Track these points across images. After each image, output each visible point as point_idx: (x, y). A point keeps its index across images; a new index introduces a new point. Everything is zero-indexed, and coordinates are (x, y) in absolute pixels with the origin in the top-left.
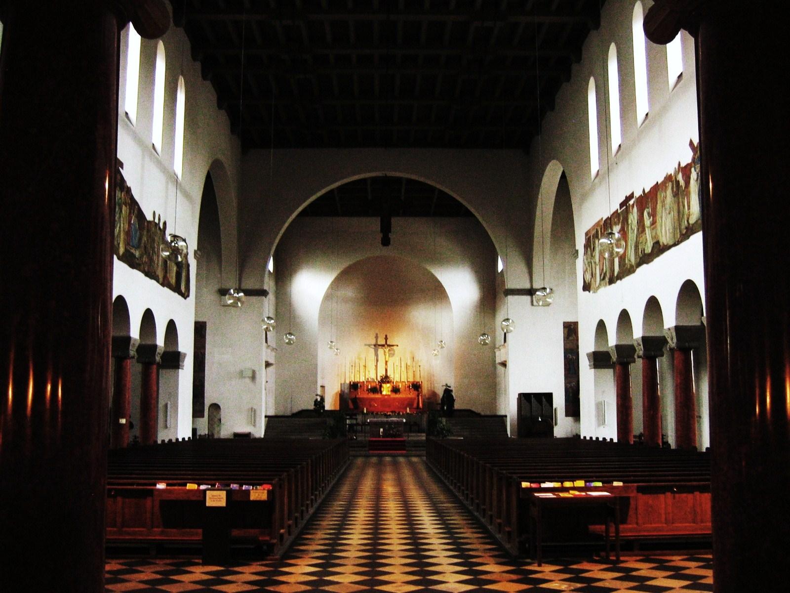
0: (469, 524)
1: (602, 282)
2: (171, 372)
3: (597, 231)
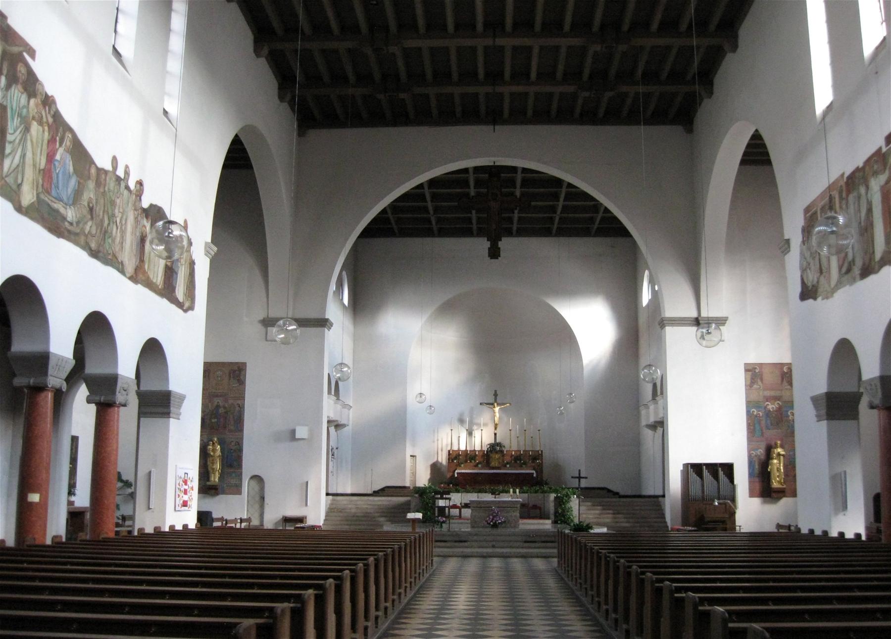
0: (570, 602)
1: (846, 277)
2: (159, 422)
3: (831, 199)
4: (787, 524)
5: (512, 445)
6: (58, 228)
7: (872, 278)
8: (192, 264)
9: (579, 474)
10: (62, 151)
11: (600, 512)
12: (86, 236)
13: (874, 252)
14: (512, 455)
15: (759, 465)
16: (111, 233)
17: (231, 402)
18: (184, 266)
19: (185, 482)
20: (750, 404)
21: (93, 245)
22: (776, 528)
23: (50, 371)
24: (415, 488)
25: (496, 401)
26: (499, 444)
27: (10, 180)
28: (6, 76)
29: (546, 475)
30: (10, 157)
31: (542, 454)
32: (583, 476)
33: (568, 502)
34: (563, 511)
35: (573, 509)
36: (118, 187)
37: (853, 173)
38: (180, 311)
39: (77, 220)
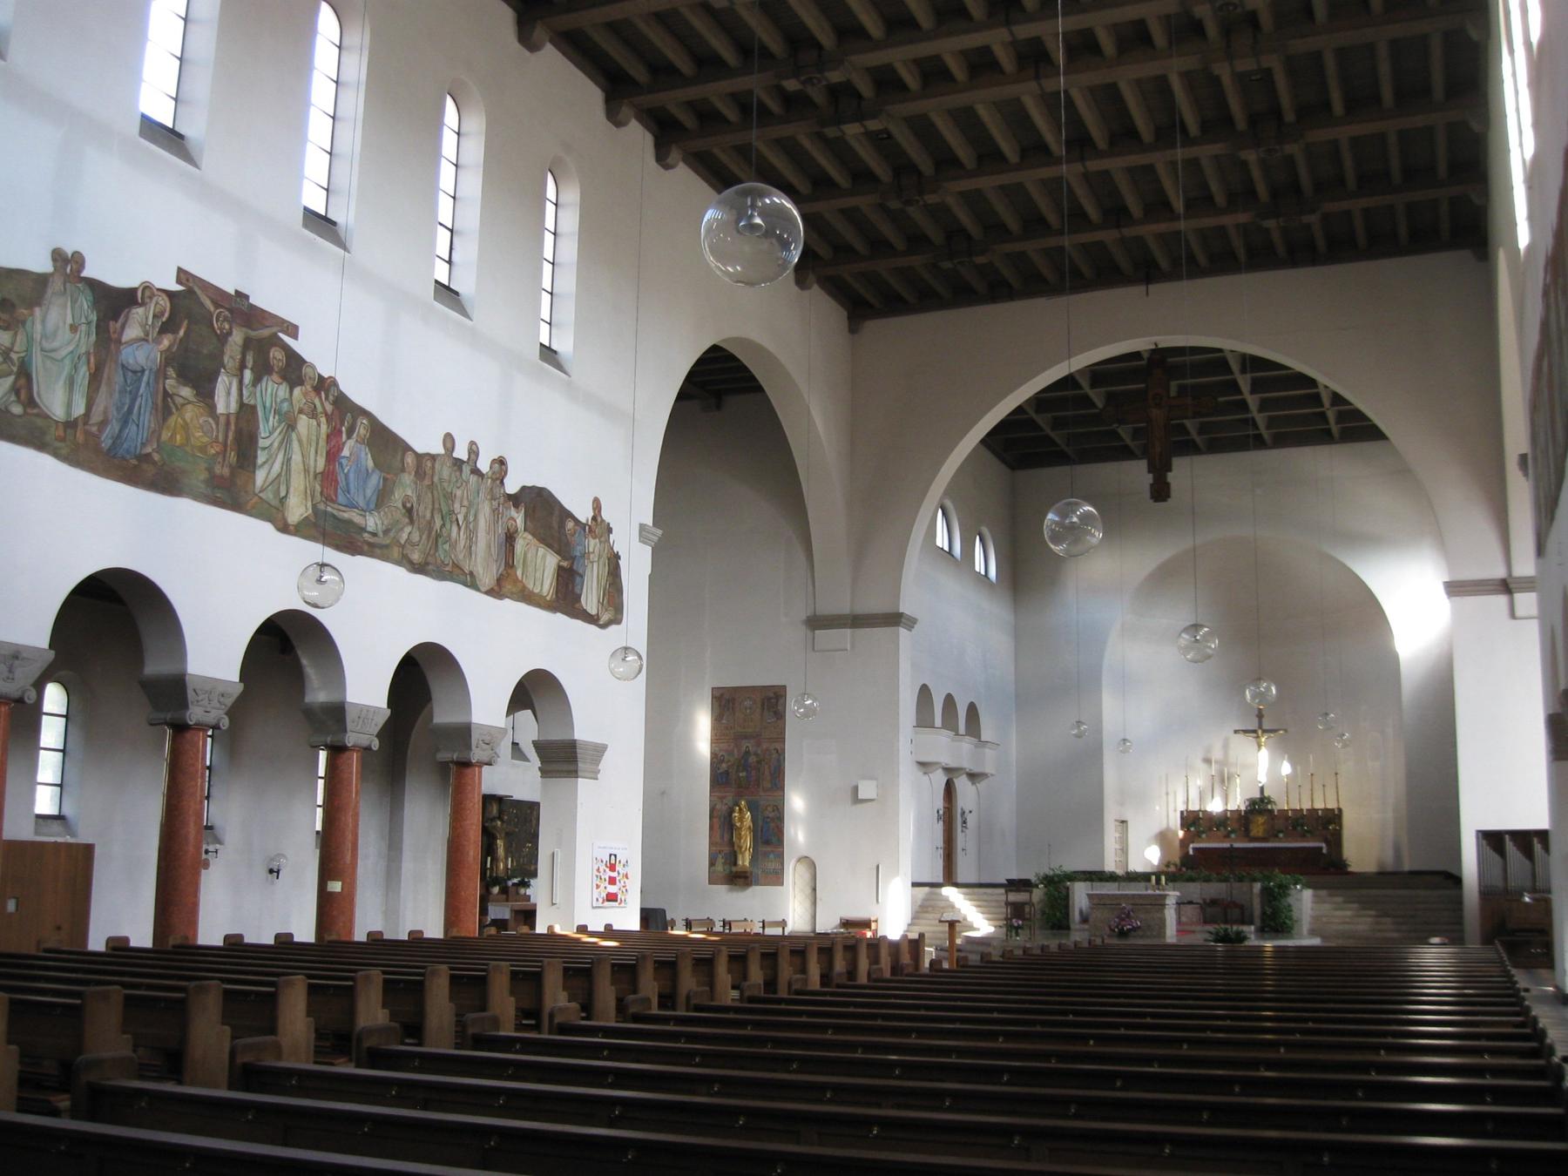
6: (351, 543)
8: (614, 561)
10: (353, 444)
12: (403, 547)
16: (449, 536)
17: (765, 746)
18: (595, 565)
19: (612, 868)
21: (416, 557)
23: (350, 726)
25: (1260, 726)
27: (268, 496)
28: (252, 369)
30: (266, 467)
36: (458, 473)
38: (593, 628)
39: (384, 528)
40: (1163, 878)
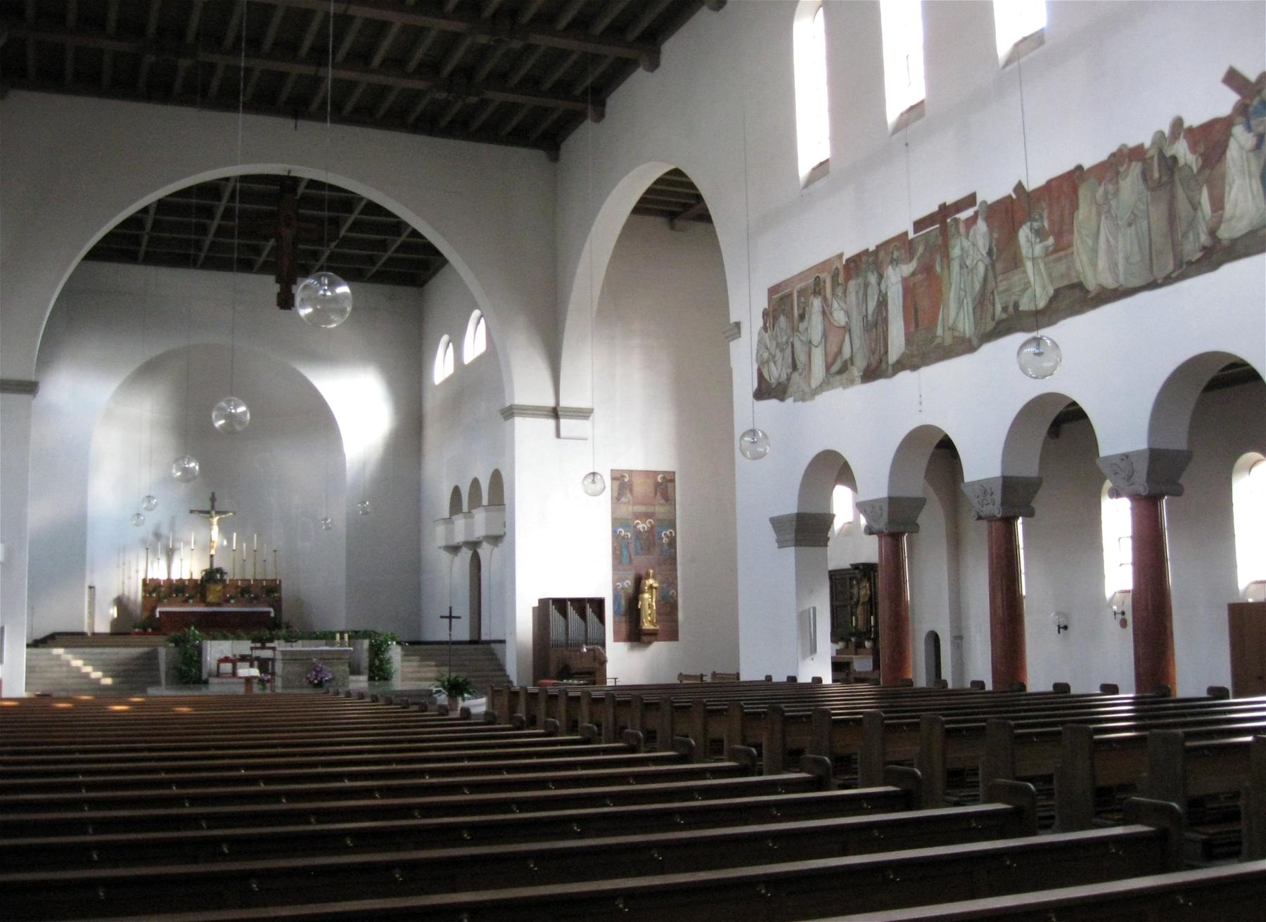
4: (698, 673)
5: (233, 571)
7: (880, 383)
9: (451, 612)
11: (419, 663)
13: (886, 352)
14: (237, 587)
15: (626, 600)
20: (617, 522)
22: (678, 679)
24: (94, 634)
25: (213, 507)
26: (219, 571)
29: (286, 617)
31: (280, 585)
32: (456, 615)
33: (387, 650)
34: (381, 661)
35: (393, 660)
37: (859, 256)
40: (346, 636)
